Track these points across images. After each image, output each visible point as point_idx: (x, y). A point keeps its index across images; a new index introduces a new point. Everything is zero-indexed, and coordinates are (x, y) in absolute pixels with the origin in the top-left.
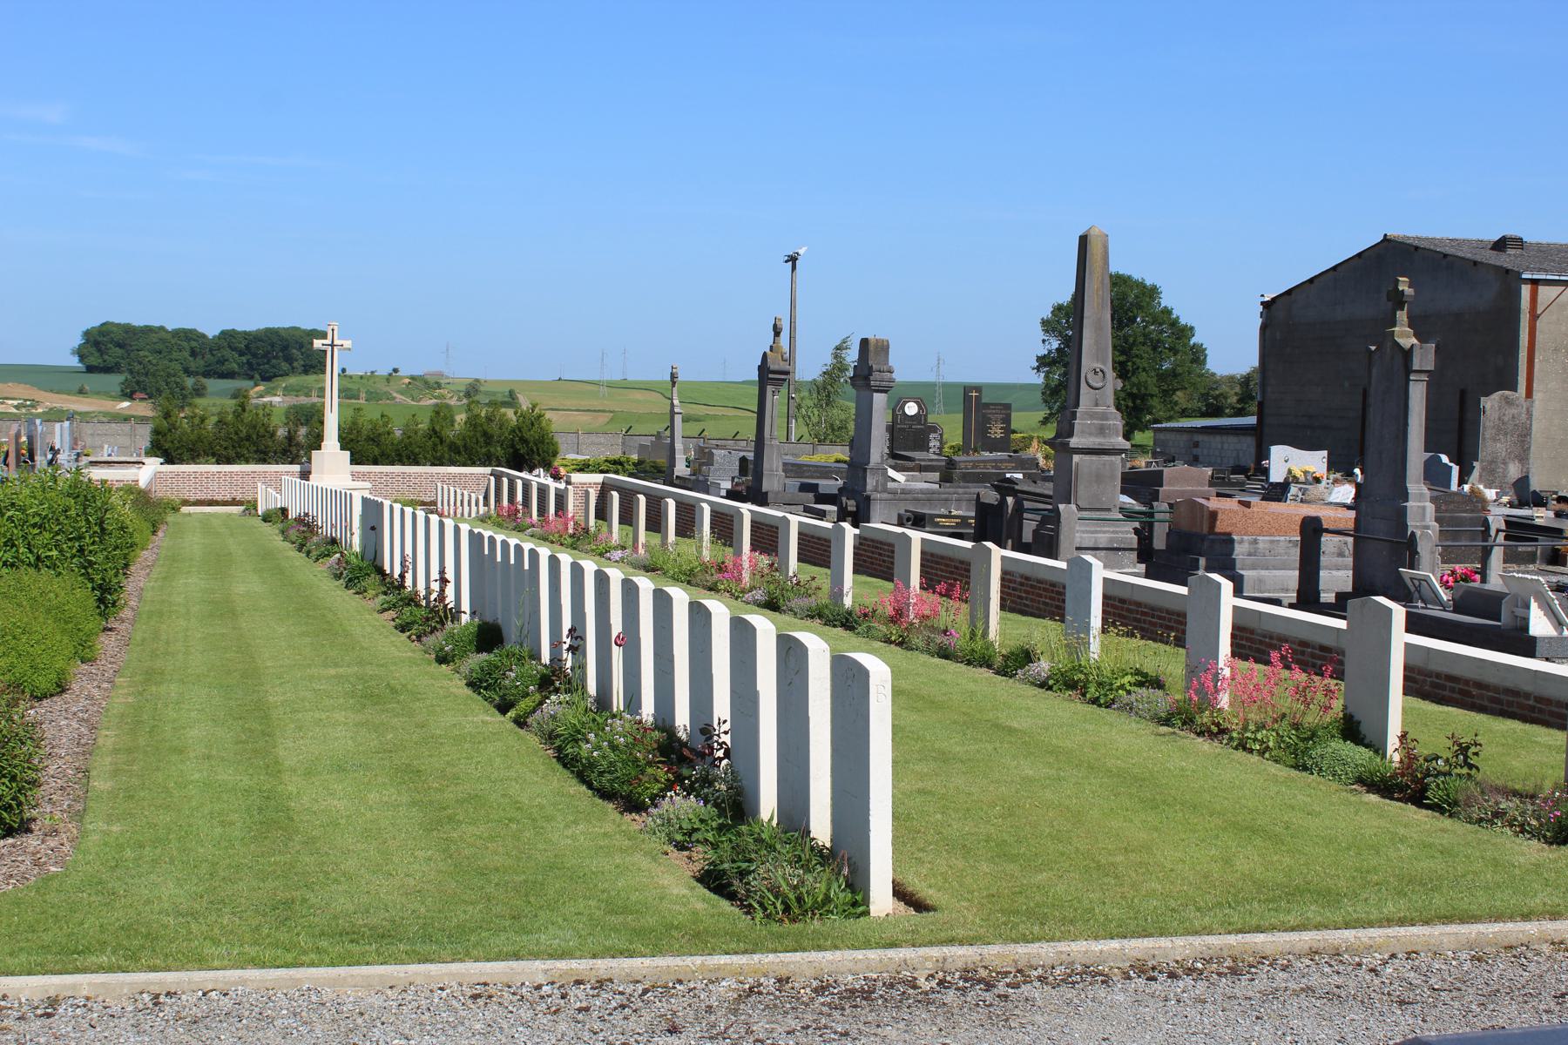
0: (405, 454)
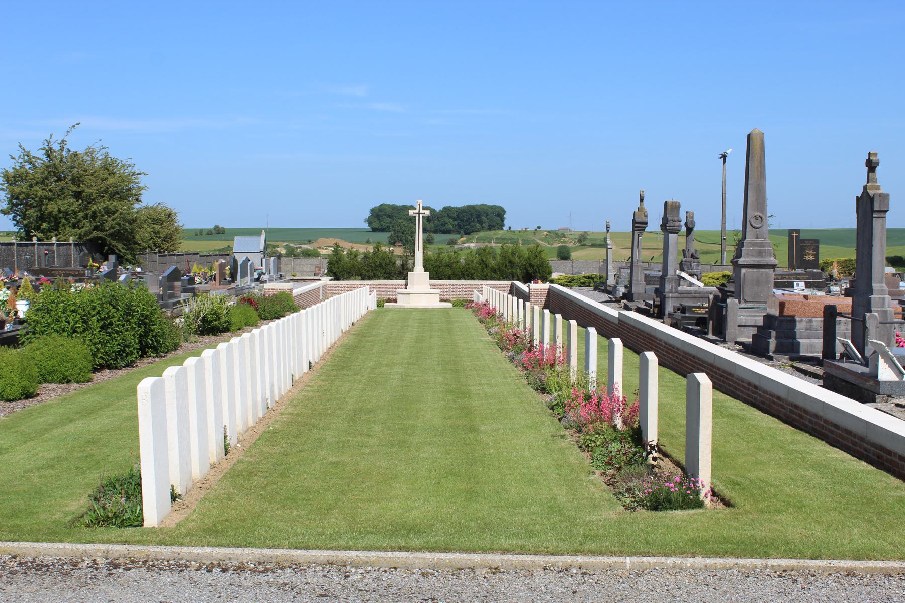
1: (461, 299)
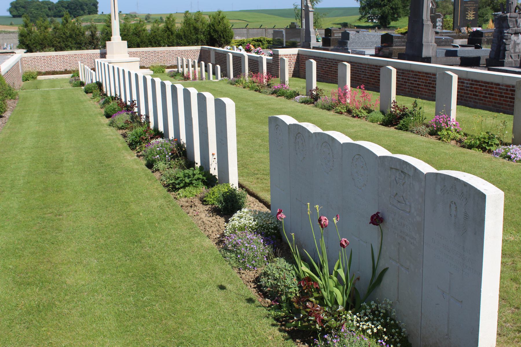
0: (153, 41)
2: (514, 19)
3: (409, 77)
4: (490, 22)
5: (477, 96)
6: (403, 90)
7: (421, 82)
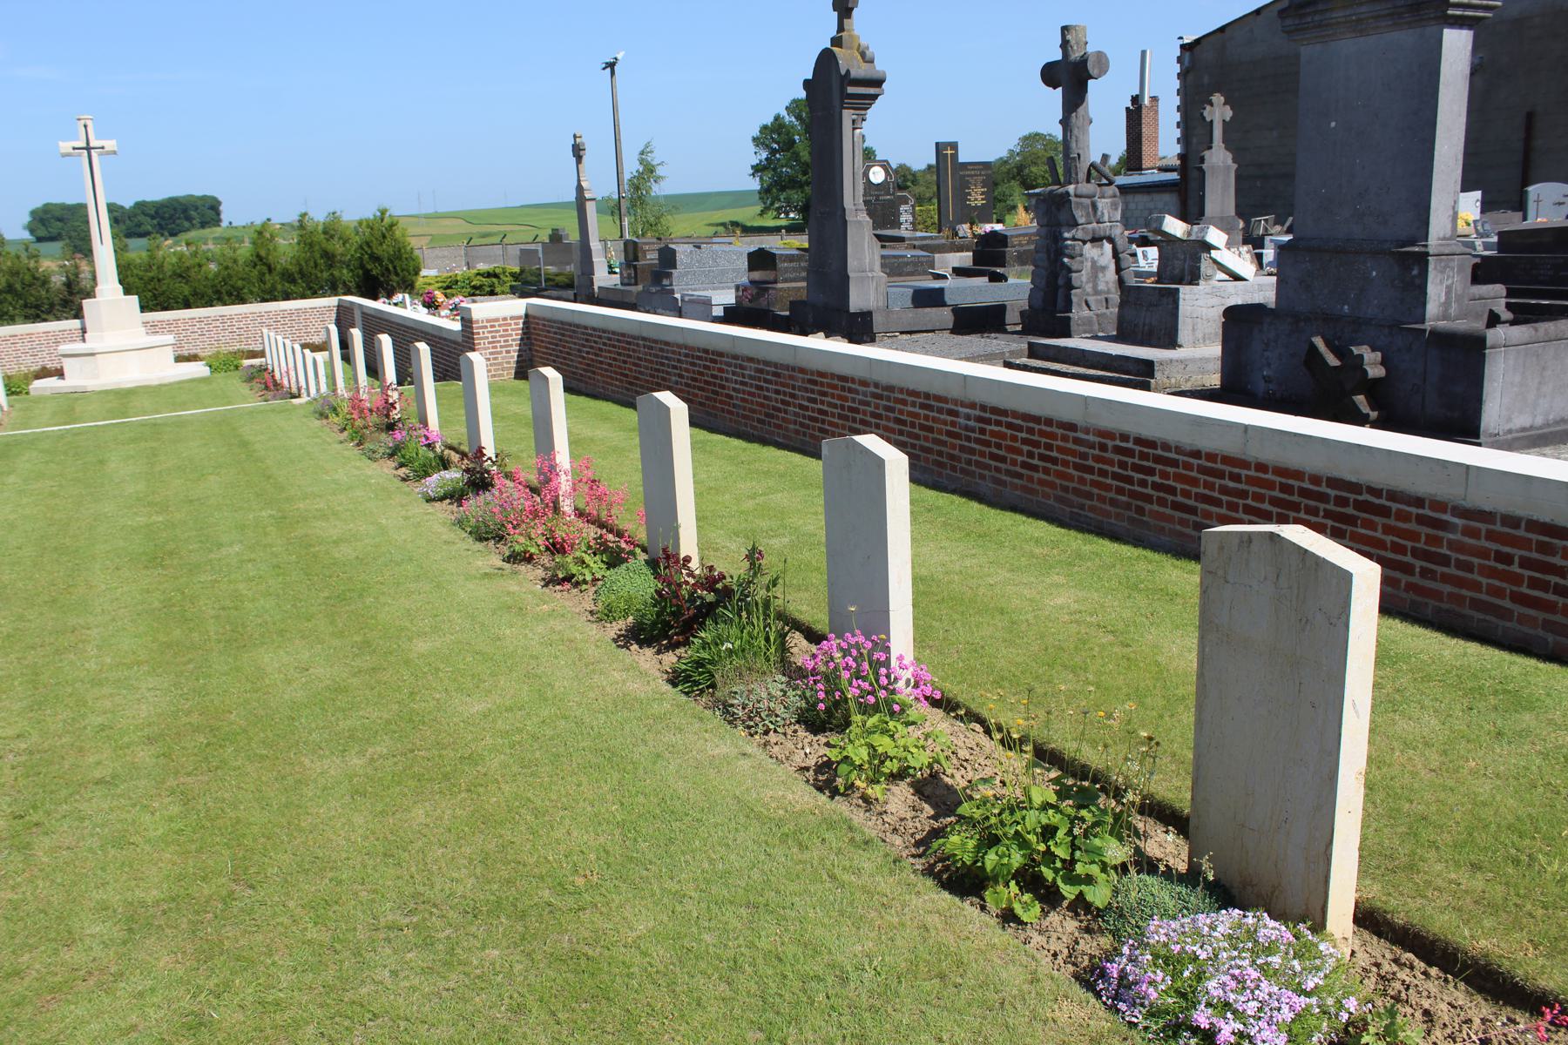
1: (224, 349)
2: (1087, 201)
3: (794, 387)
4: (1021, 209)
5: (1003, 459)
6: (779, 427)
7: (830, 404)
